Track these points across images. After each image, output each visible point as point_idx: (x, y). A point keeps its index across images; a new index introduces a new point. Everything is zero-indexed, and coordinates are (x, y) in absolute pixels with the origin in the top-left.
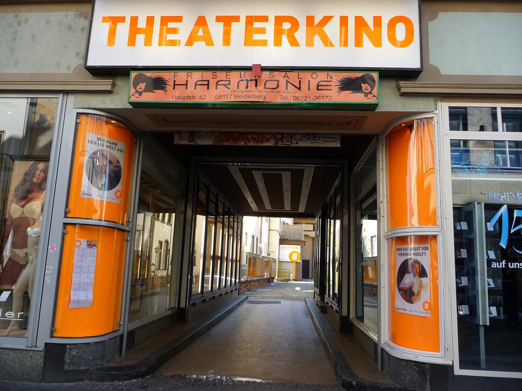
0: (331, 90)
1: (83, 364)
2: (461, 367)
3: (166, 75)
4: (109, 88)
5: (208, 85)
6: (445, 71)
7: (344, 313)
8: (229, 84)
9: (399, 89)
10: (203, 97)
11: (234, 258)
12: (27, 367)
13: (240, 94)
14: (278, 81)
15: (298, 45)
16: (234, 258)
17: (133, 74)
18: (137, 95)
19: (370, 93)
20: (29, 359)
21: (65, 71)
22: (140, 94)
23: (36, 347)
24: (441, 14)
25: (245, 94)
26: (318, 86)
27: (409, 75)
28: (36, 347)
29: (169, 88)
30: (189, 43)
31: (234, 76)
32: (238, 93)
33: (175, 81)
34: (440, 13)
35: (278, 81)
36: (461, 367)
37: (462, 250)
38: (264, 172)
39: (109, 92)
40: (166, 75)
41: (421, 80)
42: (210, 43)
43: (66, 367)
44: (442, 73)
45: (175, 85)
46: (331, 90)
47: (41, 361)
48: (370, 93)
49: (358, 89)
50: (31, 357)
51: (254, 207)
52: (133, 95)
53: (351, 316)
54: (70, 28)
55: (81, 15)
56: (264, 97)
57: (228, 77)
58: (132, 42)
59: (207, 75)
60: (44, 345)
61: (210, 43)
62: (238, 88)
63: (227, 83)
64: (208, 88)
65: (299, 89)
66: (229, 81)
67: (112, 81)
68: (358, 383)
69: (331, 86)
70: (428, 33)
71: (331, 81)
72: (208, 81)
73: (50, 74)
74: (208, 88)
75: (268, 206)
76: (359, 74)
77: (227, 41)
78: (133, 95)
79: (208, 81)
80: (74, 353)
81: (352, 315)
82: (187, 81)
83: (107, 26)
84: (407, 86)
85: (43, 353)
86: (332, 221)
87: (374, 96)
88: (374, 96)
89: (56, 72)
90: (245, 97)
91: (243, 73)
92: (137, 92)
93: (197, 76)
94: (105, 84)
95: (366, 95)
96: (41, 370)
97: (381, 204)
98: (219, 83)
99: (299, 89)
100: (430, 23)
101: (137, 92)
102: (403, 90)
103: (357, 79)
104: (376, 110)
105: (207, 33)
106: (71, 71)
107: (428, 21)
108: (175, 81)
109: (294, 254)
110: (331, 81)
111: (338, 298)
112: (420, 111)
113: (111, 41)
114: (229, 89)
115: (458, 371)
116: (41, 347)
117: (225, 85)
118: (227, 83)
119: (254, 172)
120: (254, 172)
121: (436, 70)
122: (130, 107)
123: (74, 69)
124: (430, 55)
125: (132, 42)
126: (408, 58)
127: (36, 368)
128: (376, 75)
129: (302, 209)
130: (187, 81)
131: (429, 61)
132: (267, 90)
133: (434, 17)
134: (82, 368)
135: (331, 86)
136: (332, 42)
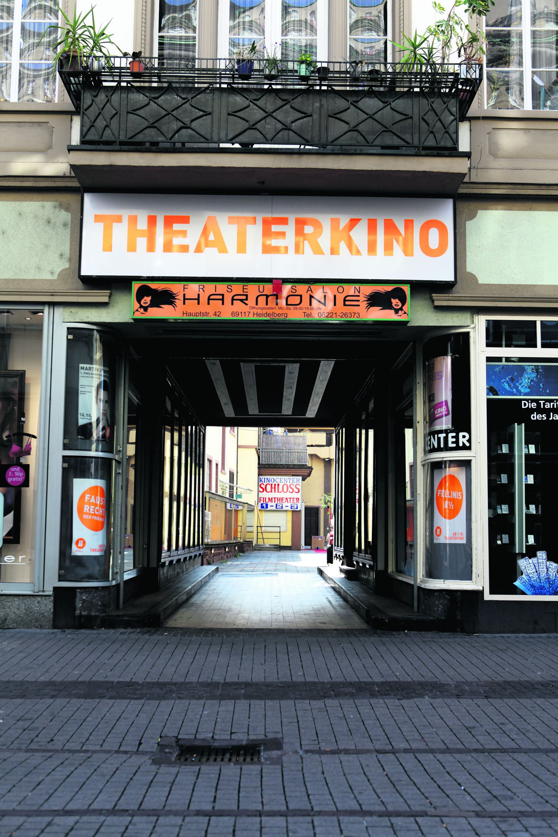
0: (359, 305)
1: (93, 610)
2: (491, 593)
3: (176, 288)
4: (106, 299)
5: (223, 300)
6: (482, 280)
7: (381, 567)
8: (247, 299)
9: (433, 301)
10: (217, 314)
11: (175, 504)
12: (35, 613)
13: (260, 311)
14: (301, 296)
15: (324, 254)
16: (175, 504)
17: (136, 286)
18: (142, 310)
19: (401, 309)
20: (37, 605)
21: (48, 277)
22: (146, 309)
23: (43, 591)
24: (481, 213)
25: (265, 311)
26: (345, 300)
27: (443, 287)
28: (43, 591)
29: (179, 302)
30: (198, 250)
31: (253, 290)
32: (257, 310)
33: (184, 295)
34: (479, 211)
35: (301, 296)
36: (491, 593)
37: (502, 475)
38: (258, 364)
39: (104, 305)
40: (176, 288)
41: (457, 291)
42: (223, 249)
43: (78, 612)
44: (480, 282)
45: (185, 299)
46: (359, 305)
47: (51, 606)
48: (401, 309)
49: (388, 306)
50: (38, 602)
51: (229, 412)
52: (137, 310)
53: (390, 570)
54: (49, 222)
55: (61, 206)
56: (286, 315)
57: (245, 290)
58: (132, 248)
59: (222, 288)
60: (52, 590)
61: (223, 249)
62: (257, 304)
63: (244, 297)
64: (223, 304)
65: (324, 304)
66: (247, 296)
67: (109, 291)
68: (390, 619)
69: (359, 301)
70: (465, 235)
71: (359, 296)
72: (223, 295)
73: (30, 280)
74: (223, 304)
75: (253, 409)
76: (389, 288)
77: (242, 248)
78: (137, 310)
79: (223, 295)
80: (84, 598)
81: (391, 569)
82: (199, 295)
83: (100, 226)
84: (441, 300)
85: (52, 598)
86: (363, 431)
87: (405, 313)
88: (405, 313)
89: (37, 278)
90: (266, 315)
91: (261, 285)
92: (141, 307)
93: (210, 288)
94: (101, 296)
95: (397, 311)
96: (52, 616)
97: (418, 424)
98: (235, 298)
99: (324, 304)
100: (469, 225)
101: (141, 307)
102: (437, 303)
103: (387, 293)
104: (408, 325)
105: (218, 235)
106: (55, 277)
107: (466, 221)
108: (184, 295)
109: (81, 546)
110: (359, 296)
111: (371, 548)
112: (455, 325)
113: (108, 247)
114: (247, 304)
115: (488, 597)
116: (49, 591)
117: (242, 300)
118: (244, 297)
119: (242, 364)
120: (242, 364)
121: (473, 278)
122: (132, 321)
123: (59, 275)
124: (467, 261)
125: (132, 248)
126: (441, 270)
127: (46, 614)
128: (407, 289)
129: (312, 412)
130: (199, 295)
131: (466, 268)
132: (289, 306)
133: (472, 216)
134: (93, 614)
135: (359, 301)
136: (359, 249)
